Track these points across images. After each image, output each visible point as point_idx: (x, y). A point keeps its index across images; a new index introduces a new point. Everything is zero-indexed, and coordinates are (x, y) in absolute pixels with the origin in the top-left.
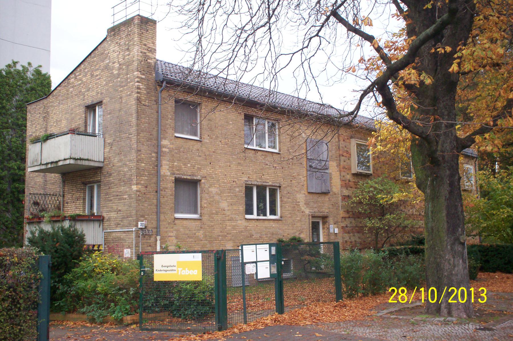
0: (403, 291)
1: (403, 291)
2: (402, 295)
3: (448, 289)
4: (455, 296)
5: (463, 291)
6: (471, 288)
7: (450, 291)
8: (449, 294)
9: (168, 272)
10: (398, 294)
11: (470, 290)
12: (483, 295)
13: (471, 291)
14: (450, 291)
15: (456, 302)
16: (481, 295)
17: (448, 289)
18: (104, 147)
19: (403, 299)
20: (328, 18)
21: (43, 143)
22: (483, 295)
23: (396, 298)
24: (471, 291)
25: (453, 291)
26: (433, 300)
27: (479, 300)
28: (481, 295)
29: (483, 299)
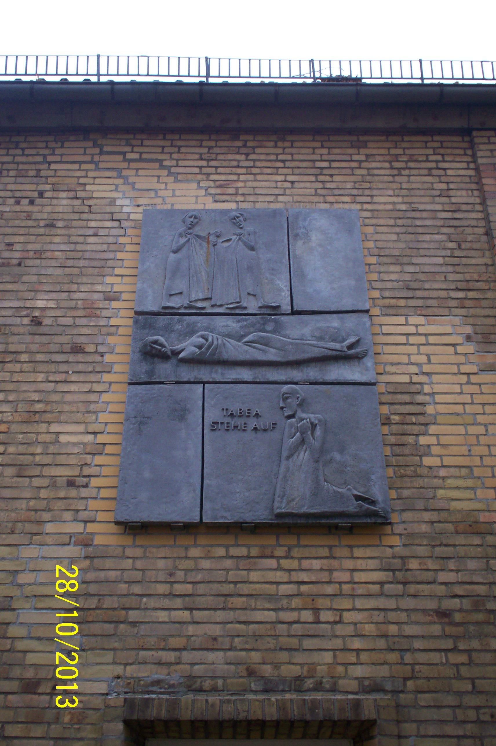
0: (72, 586)
1: (72, 586)
2: (68, 587)
3: (75, 651)
4: (67, 662)
5: (72, 673)
6: (77, 685)
7: (73, 654)
8: (68, 653)
9: (336, 206)
10: (68, 579)
11: (75, 612)
12: (67, 703)
13: (73, 613)
14: (73, 654)
15: (57, 576)
16: (67, 700)
17: (75, 651)
18: (84, 402)
19: (62, 586)
20: (9, 454)
21: (132, 337)
22: (67, 703)
23: (63, 576)
24: (73, 613)
25: (73, 571)
26: (60, 629)
27: (60, 697)
28: (67, 700)
29: (62, 702)
